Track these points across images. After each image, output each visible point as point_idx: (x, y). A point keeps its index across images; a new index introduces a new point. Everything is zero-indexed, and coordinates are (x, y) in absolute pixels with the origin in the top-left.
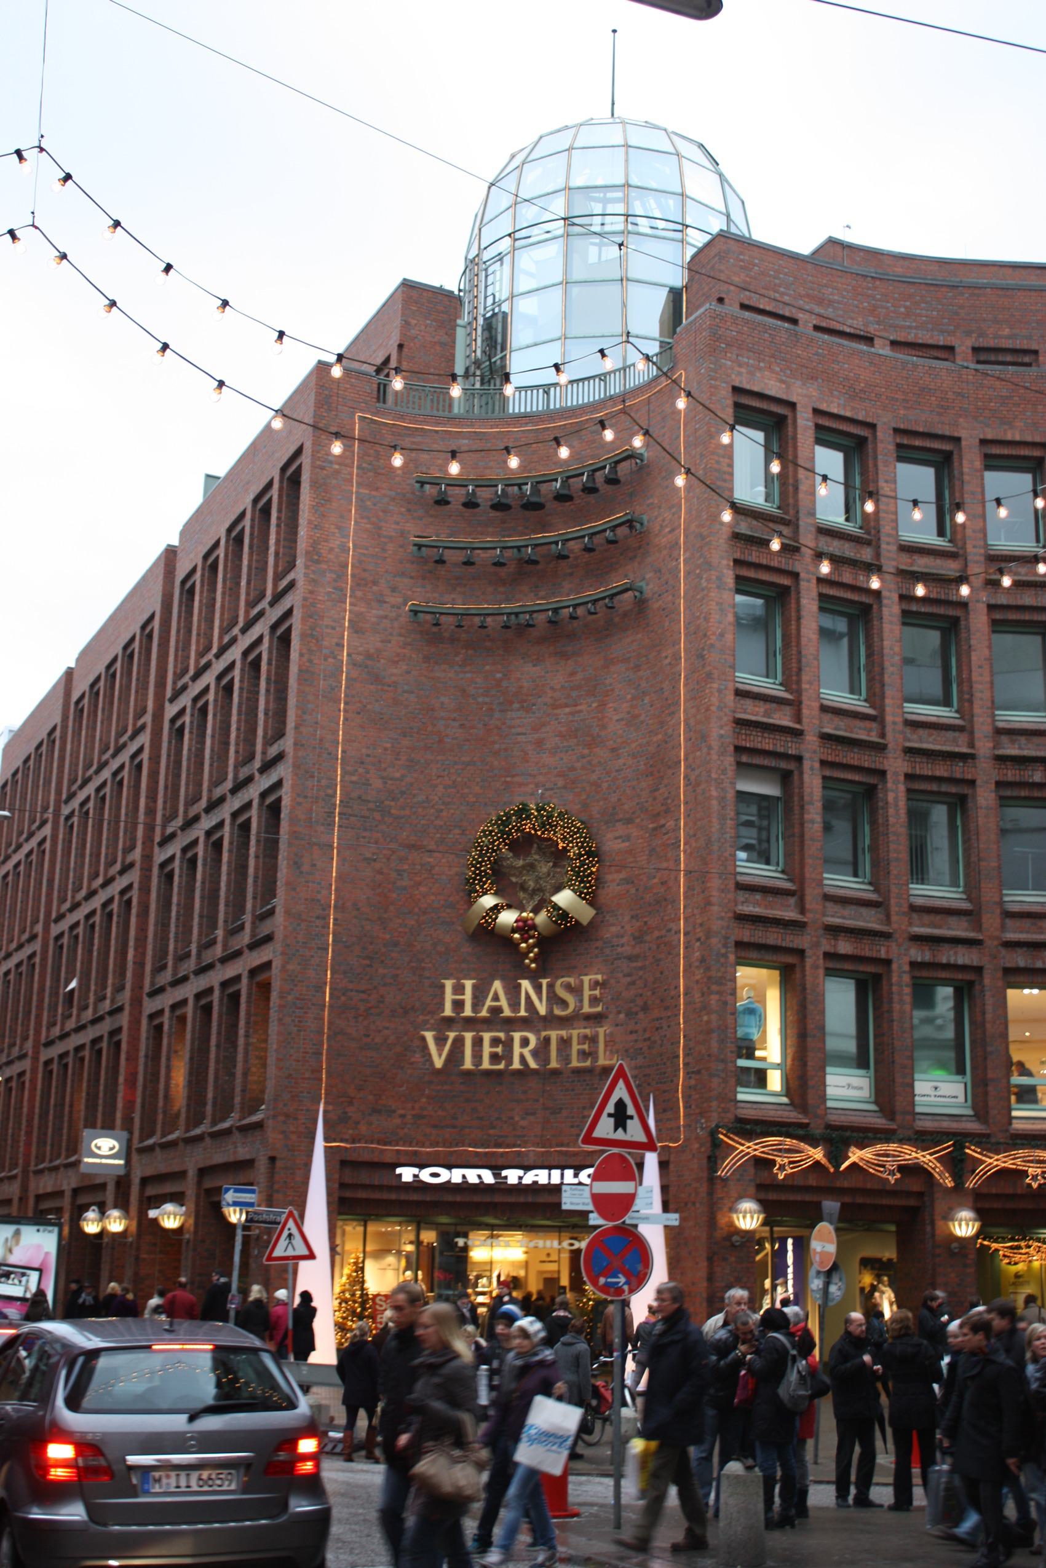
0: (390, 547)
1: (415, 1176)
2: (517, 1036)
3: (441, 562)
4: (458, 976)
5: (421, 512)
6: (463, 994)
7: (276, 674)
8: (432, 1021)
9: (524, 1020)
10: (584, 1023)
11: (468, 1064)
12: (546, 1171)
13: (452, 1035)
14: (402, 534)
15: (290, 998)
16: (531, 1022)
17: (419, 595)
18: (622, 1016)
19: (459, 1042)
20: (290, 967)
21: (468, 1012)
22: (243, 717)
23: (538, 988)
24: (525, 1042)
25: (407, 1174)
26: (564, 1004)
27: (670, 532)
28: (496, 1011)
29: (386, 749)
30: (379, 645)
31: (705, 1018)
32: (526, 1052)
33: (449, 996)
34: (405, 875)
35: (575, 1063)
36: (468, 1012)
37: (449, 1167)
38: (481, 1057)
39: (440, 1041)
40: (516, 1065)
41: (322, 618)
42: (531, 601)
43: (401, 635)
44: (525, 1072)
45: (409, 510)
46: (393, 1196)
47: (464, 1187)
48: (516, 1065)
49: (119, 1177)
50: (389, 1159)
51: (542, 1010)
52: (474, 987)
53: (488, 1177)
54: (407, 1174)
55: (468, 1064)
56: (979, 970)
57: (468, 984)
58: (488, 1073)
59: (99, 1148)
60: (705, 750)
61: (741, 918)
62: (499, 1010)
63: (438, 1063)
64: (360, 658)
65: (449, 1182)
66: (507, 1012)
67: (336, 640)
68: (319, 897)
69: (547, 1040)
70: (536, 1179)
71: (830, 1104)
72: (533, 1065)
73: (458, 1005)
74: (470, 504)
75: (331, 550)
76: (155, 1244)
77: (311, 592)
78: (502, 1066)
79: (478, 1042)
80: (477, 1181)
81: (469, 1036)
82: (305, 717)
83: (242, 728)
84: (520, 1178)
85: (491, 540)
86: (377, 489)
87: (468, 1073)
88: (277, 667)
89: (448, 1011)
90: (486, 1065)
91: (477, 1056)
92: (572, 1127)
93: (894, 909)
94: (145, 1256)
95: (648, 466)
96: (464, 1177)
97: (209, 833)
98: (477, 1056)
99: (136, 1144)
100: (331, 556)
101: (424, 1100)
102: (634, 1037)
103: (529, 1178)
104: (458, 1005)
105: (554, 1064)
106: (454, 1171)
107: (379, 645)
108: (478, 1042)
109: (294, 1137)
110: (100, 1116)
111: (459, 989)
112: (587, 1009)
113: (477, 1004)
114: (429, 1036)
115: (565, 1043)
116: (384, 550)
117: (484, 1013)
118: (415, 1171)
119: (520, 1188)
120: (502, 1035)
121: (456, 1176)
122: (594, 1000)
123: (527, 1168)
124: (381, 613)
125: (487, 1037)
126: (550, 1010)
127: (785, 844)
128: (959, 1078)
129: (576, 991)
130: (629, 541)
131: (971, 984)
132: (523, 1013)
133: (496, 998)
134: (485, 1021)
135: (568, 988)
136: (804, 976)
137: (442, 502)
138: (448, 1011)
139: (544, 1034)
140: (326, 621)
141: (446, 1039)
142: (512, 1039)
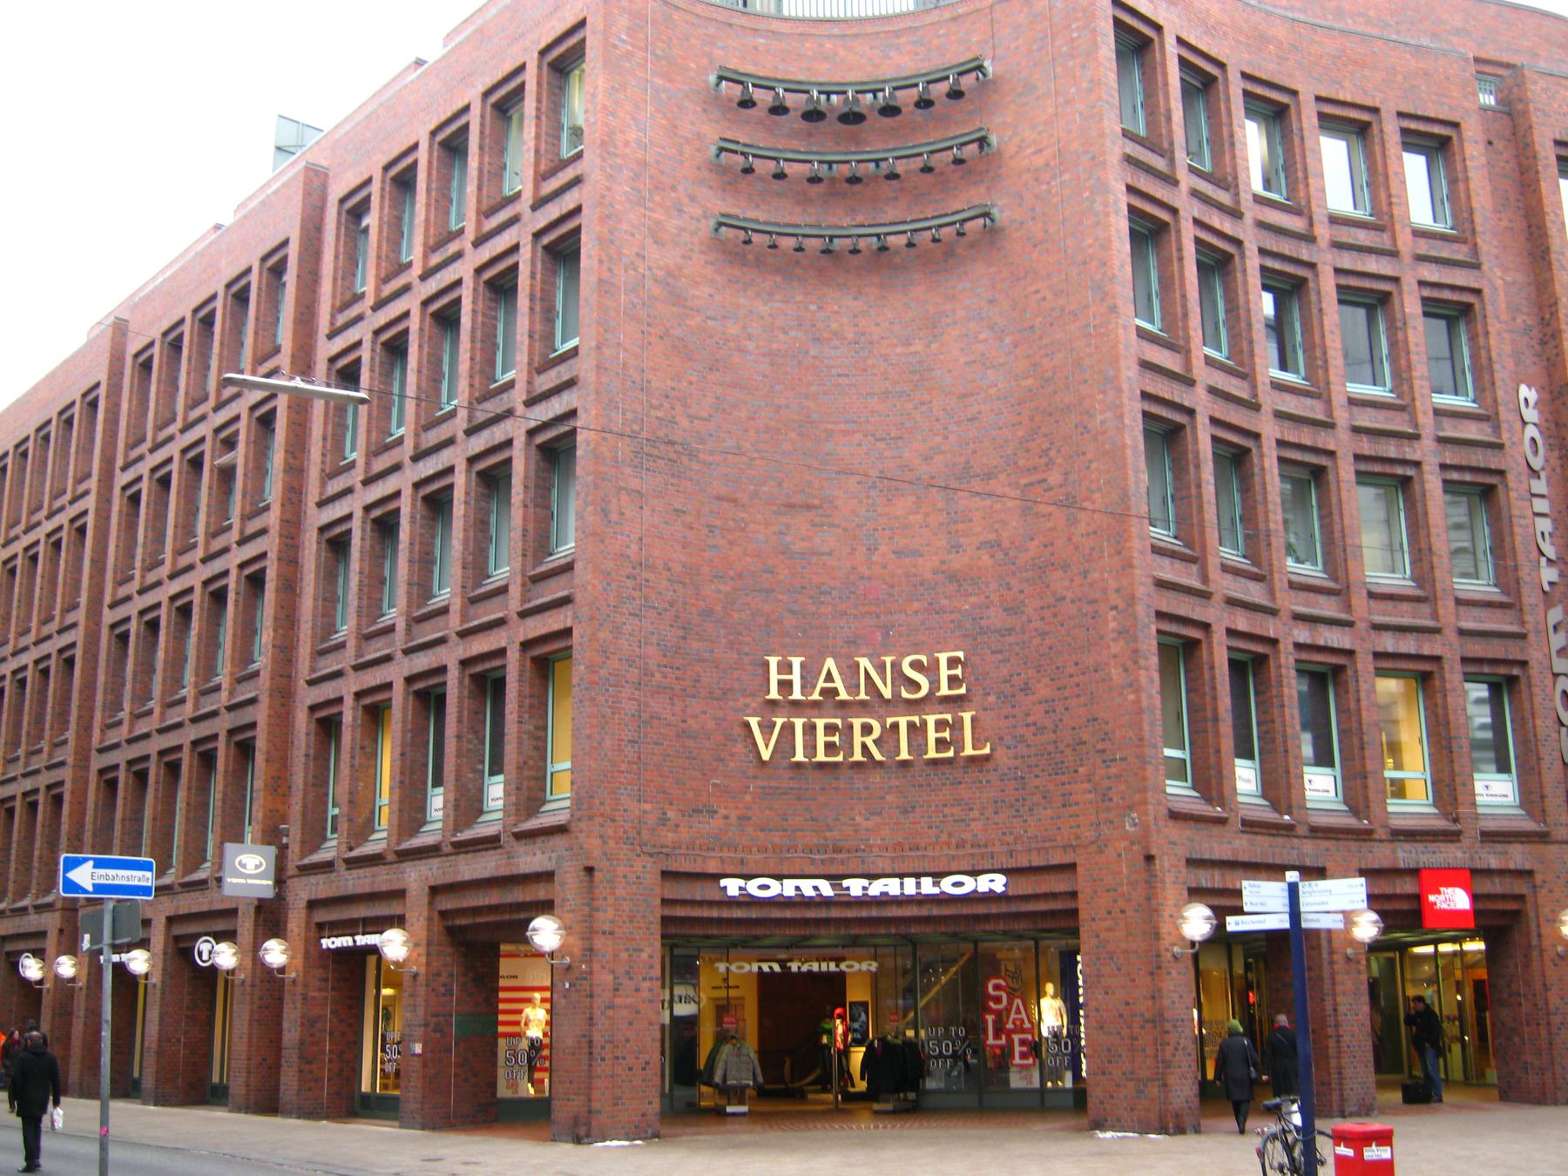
0: (687, 150)
1: (865, 888)
2: (857, 723)
3: (748, 171)
4: (785, 651)
5: (717, 113)
6: (791, 673)
7: (542, 290)
8: (754, 705)
9: (863, 703)
10: (941, 708)
11: (800, 756)
12: (897, 880)
13: (779, 721)
14: (699, 136)
15: (603, 672)
16: (877, 704)
17: (721, 204)
18: (992, 698)
19: (788, 729)
20: (601, 635)
21: (797, 695)
22: (479, 345)
23: (881, 668)
24: (867, 730)
25: (732, 886)
26: (916, 686)
27: (1035, 153)
28: (830, 693)
29: (691, 383)
30: (680, 261)
31: (1131, 697)
32: (869, 741)
33: (774, 677)
34: (717, 531)
35: (932, 753)
36: (797, 695)
37: (779, 877)
38: (815, 747)
39: (767, 728)
40: (858, 756)
41: (620, 221)
42: (845, 221)
43: (702, 252)
44: (870, 763)
45: (705, 111)
46: (715, 913)
47: (801, 902)
48: (858, 756)
49: (260, 900)
50: (712, 867)
51: (887, 693)
52: (803, 665)
53: (826, 889)
54: (732, 886)
55: (800, 756)
56: (1350, 653)
57: (796, 662)
58: (821, 765)
59: (244, 866)
60: (1111, 393)
61: (1161, 584)
62: (835, 692)
63: (766, 755)
64: (660, 273)
65: (975, 891)
66: (843, 695)
67: (635, 249)
68: (629, 552)
69: (895, 726)
70: (885, 889)
71: (1240, 799)
72: (878, 757)
73: (785, 686)
74: (779, 109)
75: (627, 144)
76: (326, 980)
77: (609, 189)
78: (951, 754)
79: (810, 729)
80: (812, 893)
81: (799, 723)
82: (609, 336)
83: (478, 358)
84: (865, 888)
85: (804, 154)
86: (670, 81)
87: (799, 765)
88: (543, 282)
89: (774, 694)
90: (821, 756)
91: (810, 748)
92: (930, 828)
93: (1278, 585)
94: (315, 994)
95: (994, 82)
96: (798, 888)
97: (26, 549)
98: (810, 748)
99: (294, 859)
100: (628, 151)
101: (748, 798)
102: (1011, 721)
103: (876, 888)
104: (785, 686)
105: (904, 755)
106: (785, 881)
107: (680, 261)
108: (810, 729)
109: (612, 843)
110: (117, 833)
111: (786, 667)
112: (944, 690)
113: (807, 686)
114: (754, 722)
115: (916, 731)
116: (681, 152)
117: (816, 696)
118: (741, 882)
119: (865, 902)
120: (948, 717)
121: (789, 888)
122: (953, 681)
123: (872, 877)
124: (680, 223)
125: (820, 724)
126: (896, 694)
127: (1177, 507)
128: (1328, 770)
129: (931, 670)
130: (976, 158)
131: (1338, 670)
132: (863, 696)
133: (829, 678)
134: (815, 704)
135: (916, 666)
136: (1211, 653)
137: (747, 103)
138: (774, 694)
139: (890, 721)
140: (625, 226)
141: (774, 724)
142: (851, 727)
